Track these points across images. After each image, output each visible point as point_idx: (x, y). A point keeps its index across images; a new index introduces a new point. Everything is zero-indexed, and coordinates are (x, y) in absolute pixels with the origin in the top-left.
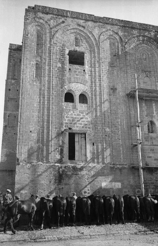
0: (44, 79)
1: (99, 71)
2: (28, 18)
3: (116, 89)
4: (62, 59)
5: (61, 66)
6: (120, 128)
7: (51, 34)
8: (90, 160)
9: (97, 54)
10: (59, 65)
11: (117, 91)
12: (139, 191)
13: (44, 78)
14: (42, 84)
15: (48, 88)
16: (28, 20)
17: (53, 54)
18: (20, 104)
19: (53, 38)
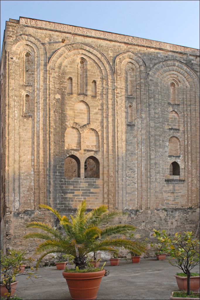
0: (38, 115)
1: (113, 105)
2: (11, 35)
3: (134, 125)
4: (63, 89)
5: (60, 98)
6: (136, 170)
7: (45, 86)
8: (87, 67)
9: (111, 82)
10: (58, 96)
11: (136, 128)
12: (140, 62)
13: (38, 113)
14: (36, 121)
15: (44, 151)
16: (11, 38)
17: (49, 82)
18: (7, 145)
19: (49, 62)
